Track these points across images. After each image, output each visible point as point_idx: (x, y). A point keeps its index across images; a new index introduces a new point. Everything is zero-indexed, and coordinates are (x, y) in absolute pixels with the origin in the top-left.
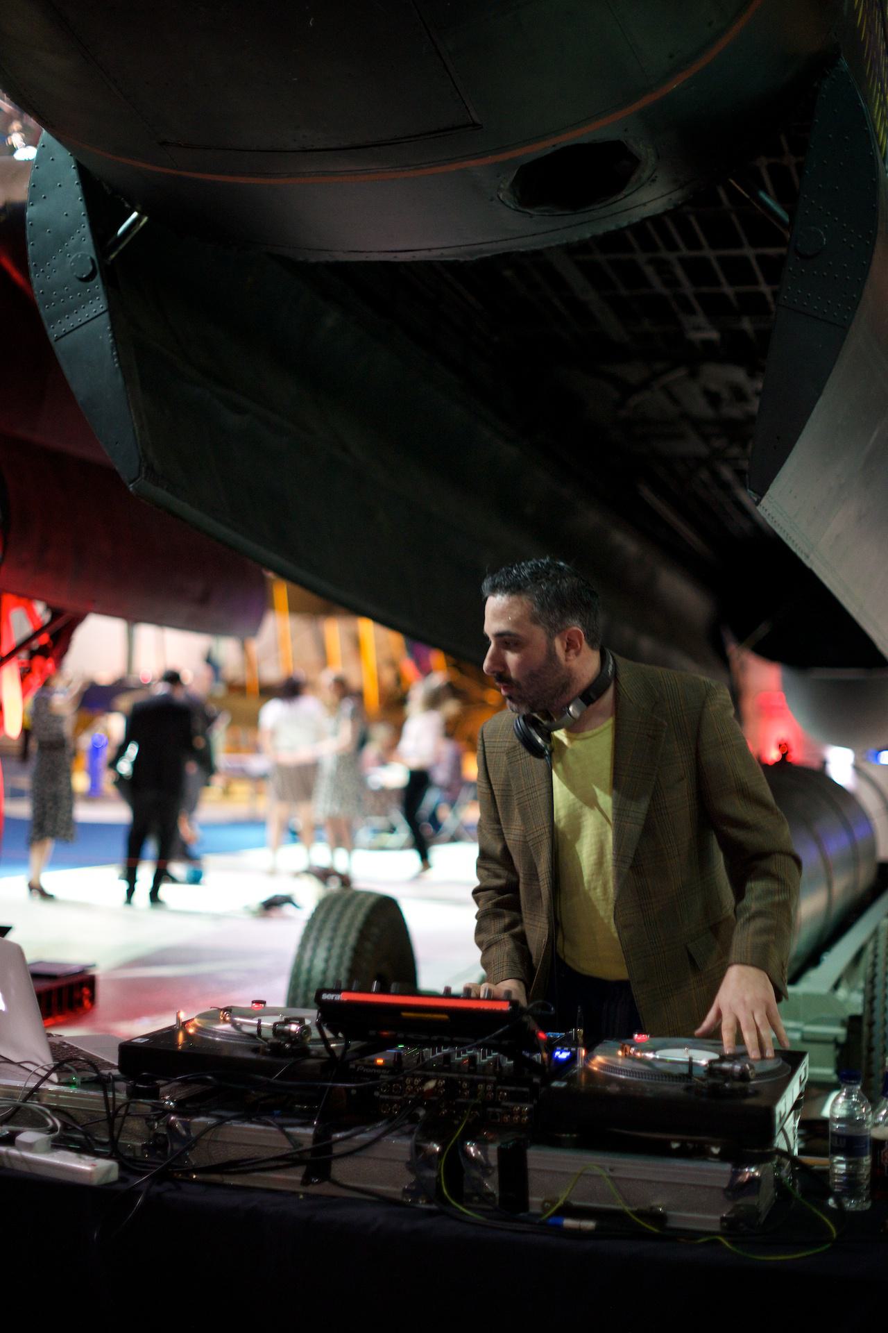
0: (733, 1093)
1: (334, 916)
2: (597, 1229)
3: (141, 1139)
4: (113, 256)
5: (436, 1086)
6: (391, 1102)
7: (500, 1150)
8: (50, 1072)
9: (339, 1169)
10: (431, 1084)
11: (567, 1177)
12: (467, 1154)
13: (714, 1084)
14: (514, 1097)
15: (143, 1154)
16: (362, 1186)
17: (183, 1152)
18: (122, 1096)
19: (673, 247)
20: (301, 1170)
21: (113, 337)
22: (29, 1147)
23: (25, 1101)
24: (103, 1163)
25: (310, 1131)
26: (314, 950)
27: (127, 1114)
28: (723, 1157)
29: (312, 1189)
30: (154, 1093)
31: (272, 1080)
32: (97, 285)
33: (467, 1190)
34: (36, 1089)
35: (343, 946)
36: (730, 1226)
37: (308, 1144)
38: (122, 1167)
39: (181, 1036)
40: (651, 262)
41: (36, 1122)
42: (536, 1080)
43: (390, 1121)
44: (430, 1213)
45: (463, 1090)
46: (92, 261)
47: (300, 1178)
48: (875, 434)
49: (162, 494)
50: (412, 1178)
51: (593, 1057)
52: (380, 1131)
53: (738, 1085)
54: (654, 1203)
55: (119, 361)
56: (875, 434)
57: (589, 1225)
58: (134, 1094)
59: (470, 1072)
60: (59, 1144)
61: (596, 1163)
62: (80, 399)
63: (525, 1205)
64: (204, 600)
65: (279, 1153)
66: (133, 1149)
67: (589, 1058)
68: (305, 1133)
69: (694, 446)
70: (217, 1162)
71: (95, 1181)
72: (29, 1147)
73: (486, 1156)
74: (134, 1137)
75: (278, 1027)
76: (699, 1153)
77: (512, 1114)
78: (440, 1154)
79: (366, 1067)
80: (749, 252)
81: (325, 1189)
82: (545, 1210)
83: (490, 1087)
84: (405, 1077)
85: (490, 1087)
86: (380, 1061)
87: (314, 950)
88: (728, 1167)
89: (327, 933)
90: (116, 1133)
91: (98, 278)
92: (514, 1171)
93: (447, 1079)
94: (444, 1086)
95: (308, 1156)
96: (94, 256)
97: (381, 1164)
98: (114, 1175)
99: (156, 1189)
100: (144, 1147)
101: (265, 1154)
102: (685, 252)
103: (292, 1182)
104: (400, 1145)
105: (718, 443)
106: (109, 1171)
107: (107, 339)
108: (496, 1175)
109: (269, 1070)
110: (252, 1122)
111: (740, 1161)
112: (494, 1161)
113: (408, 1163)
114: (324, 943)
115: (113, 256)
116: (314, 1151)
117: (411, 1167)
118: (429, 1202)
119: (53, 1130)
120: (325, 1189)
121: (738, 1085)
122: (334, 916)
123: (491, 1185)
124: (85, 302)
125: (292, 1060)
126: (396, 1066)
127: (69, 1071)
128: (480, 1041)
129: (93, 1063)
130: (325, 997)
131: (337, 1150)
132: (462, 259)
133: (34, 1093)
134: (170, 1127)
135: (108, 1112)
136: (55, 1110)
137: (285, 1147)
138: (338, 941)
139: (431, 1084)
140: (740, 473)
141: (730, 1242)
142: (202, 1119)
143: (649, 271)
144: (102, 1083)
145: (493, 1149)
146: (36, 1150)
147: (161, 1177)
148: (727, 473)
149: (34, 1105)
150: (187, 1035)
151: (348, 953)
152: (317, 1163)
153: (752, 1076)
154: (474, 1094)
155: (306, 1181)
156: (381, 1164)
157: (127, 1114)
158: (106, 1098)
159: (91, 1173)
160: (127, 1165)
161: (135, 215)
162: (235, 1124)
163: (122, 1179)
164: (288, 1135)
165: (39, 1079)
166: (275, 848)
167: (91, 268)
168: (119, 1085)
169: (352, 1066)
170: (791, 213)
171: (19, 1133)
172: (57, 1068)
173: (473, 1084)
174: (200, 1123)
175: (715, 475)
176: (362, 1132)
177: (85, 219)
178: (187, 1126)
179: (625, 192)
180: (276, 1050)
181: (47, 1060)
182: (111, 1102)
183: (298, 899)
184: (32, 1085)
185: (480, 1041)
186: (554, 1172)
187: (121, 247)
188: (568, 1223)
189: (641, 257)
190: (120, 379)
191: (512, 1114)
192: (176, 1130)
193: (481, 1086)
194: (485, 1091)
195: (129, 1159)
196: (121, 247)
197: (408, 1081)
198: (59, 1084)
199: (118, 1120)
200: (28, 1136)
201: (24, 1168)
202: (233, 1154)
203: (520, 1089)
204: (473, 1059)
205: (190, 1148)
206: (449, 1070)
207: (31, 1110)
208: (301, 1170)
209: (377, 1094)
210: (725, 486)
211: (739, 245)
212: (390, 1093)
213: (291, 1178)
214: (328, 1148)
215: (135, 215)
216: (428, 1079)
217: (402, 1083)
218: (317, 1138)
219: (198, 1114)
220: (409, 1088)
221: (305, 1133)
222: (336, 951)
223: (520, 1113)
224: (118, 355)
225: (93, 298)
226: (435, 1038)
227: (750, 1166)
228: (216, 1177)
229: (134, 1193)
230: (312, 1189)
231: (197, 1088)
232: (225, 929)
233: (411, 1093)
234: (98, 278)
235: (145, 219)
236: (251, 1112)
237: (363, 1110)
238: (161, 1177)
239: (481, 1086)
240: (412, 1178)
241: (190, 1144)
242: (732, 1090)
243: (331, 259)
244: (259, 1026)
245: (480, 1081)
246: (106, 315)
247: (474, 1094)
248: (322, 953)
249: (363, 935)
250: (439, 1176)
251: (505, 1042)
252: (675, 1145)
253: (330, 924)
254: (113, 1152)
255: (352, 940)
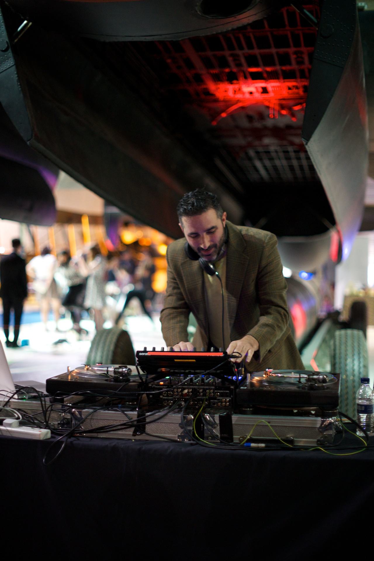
0: (318, 388)
1: (103, 338)
2: (266, 447)
3: (58, 421)
4: (16, 41)
5: (188, 392)
6: (168, 400)
7: (220, 417)
8: (14, 394)
9: (149, 428)
10: (186, 391)
11: (249, 426)
12: (205, 418)
13: (311, 384)
14: (222, 395)
15: (59, 427)
16: (159, 435)
17: (79, 425)
18: (48, 403)
19: (241, 48)
20: (133, 429)
21: (18, 77)
22: (10, 425)
23: (4, 407)
24: (44, 431)
25: (136, 413)
26: (96, 353)
27: (52, 410)
28: (316, 415)
29: (137, 438)
30: (62, 401)
31: (117, 392)
32: (10, 53)
33: (205, 435)
34: (8, 401)
35: (108, 351)
36: (320, 443)
37: (135, 418)
38: (52, 433)
39: (69, 377)
40: (232, 55)
41: (10, 415)
42: (232, 387)
43: (170, 407)
44: (192, 444)
45: (200, 393)
46: (7, 42)
47: (132, 433)
48: (347, 118)
49: (41, 147)
50: (182, 430)
51: (253, 378)
52: (166, 412)
53: (320, 385)
54: (288, 436)
55: (21, 87)
56: (347, 118)
57: (263, 445)
58: (54, 401)
59: (202, 385)
60: (21, 424)
61: (263, 420)
62: (4, 104)
63: (232, 439)
64: (30, 210)
65: (122, 422)
66: (54, 425)
67: (252, 378)
68: (134, 414)
69: (240, 141)
70: (94, 428)
71: (42, 438)
72: (10, 425)
73: (214, 419)
74: (55, 419)
75: (116, 370)
76: (307, 414)
77: (222, 402)
78: (194, 420)
79: (156, 385)
80: (274, 50)
81: (143, 437)
82: (241, 441)
83: (212, 391)
84: (174, 389)
85: (212, 391)
86: (162, 383)
87: (96, 353)
88: (319, 419)
89: (101, 345)
90: (47, 419)
91: (10, 50)
92: (226, 425)
93: (192, 389)
94: (191, 392)
95: (135, 423)
96: (7, 40)
97: (167, 427)
98: (49, 436)
99: (69, 440)
100: (59, 424)
101: (115, 423)
102: (246, 51)
103: (129, 435)
104: (177, 417)
105: (250, 139)
106: (47, 433)
107: (15, 77)
108: (218, 427)
109: (115, 388)
110: (109, 410)
111: (324, 415)
112: (217, 421)
113: (180, 424)
114: (100, 349)
115: (16, 41)
116: (138, 421)
117: (181, 425)
118: (190, 440)
119: (18, 418)
120: (143, 437)
121: (320, 385)
122: (103, 338)
123: (217, 431)
124: (4, 60)
125: (124, 383)
126: (169, 384)
127: (23, 393)
128: (207, 372)
129: (33, 389)
130: (140, 354)
131: (148, 420)
132: (174, 40)
133: (7, 403)
134: (73, 414)
135: (43, 410)
136: (19, 410)
137: (125, 420)
138: (106, 349)
139: (186, 391)
140: (257, 153)
141: (325, 450)
142: (86, 410)
143: (230, 59)
144: (38, 397)
145: (217, 417)
146: (12, 427)
147: (71, 435)
148: (252, 153)
149: (8, 408)
150: (72, 376)
151: (111, 354)
152: (139, 426)
153: (327, 380)
154: (205, 395)
155: (134, 434)
156: (167, 427)
157: (52, 410)
158: (42, 404)
159: (40, 434)
160: (54, 432)
161: (25, 22)
162: (102, 411)
163: (52, 437)
164: (126, 414)
165: (9, 398)
166: (57, 321)
167: (6, 45)
168: (47, 399)
169: (150, 385)
170: (317, 17)
171: (4, 420)
172: (17, 392)
173: (204, 390)
174: (86, 412)
175: (247, 154)
176: (159, 412)
177: (3, 24)
178: (80, 413)
179: (249, 8)
180: (116, 379)
181: (14, 389)
182: (44, 406)
183: (68, 339)
184: (7, 399)
185: (207, 372)
186: (244, 425)
187: (19, 37)
188: (253, 445)
189: (227, 53)
190: (22, 95)
191: (222, 402)
192: (76, 415)
193: (208, 391)
194: (210, 393)
195: (54, 429)
196: (19, 37)
197: (175, 390)
198: (18, 399)
199: (48, 412)
200: (8, 421)
201: (8, 435)
202: (101, 424)
203: (225, 391)
204: (203, 380)
205: (82, 423)
206: (192, 385)
207: (7, 411)
208: (133, 429)
209: (161, 397)
210: (250, 159)
211: (269, 47)
212: (168, 396)
213: (130, 432)
214: (145, 419)
215: (25, 22)
216: (184, 389)
217: (173, 391)
218: (139, 416)
219: (84, 409)
220: (176, 393)
221: (134, 414)
222: (105, 353)
223: (226, 402)
224: (20, 85)
225: (8, 59)
226: (187, 371)
227: (329, 418)
228: (94, 435)
229: (60, 443)
230: (137, 438)
231: (81, 398)
232: (52, 346)
233: (177, 395)
234: (10, 50)
235: (30, 24)
236: (108, 406)
237: (156, 404)
238: (71, 435)
239: (208, 391)
240: (182, 430)
241: (82, 421)
242: (318, 387)
243: (116, 40)
244: (107, 371)
245: (207, 389)
246: (14, 67)
247: (205, 395)
248: (99, 354)
249: (117, 346)
250: (193, 429)
251: (218, 371)
252: (295, 411)
253: (102, 341)
254: (47, 427)
255: (112, 348)
